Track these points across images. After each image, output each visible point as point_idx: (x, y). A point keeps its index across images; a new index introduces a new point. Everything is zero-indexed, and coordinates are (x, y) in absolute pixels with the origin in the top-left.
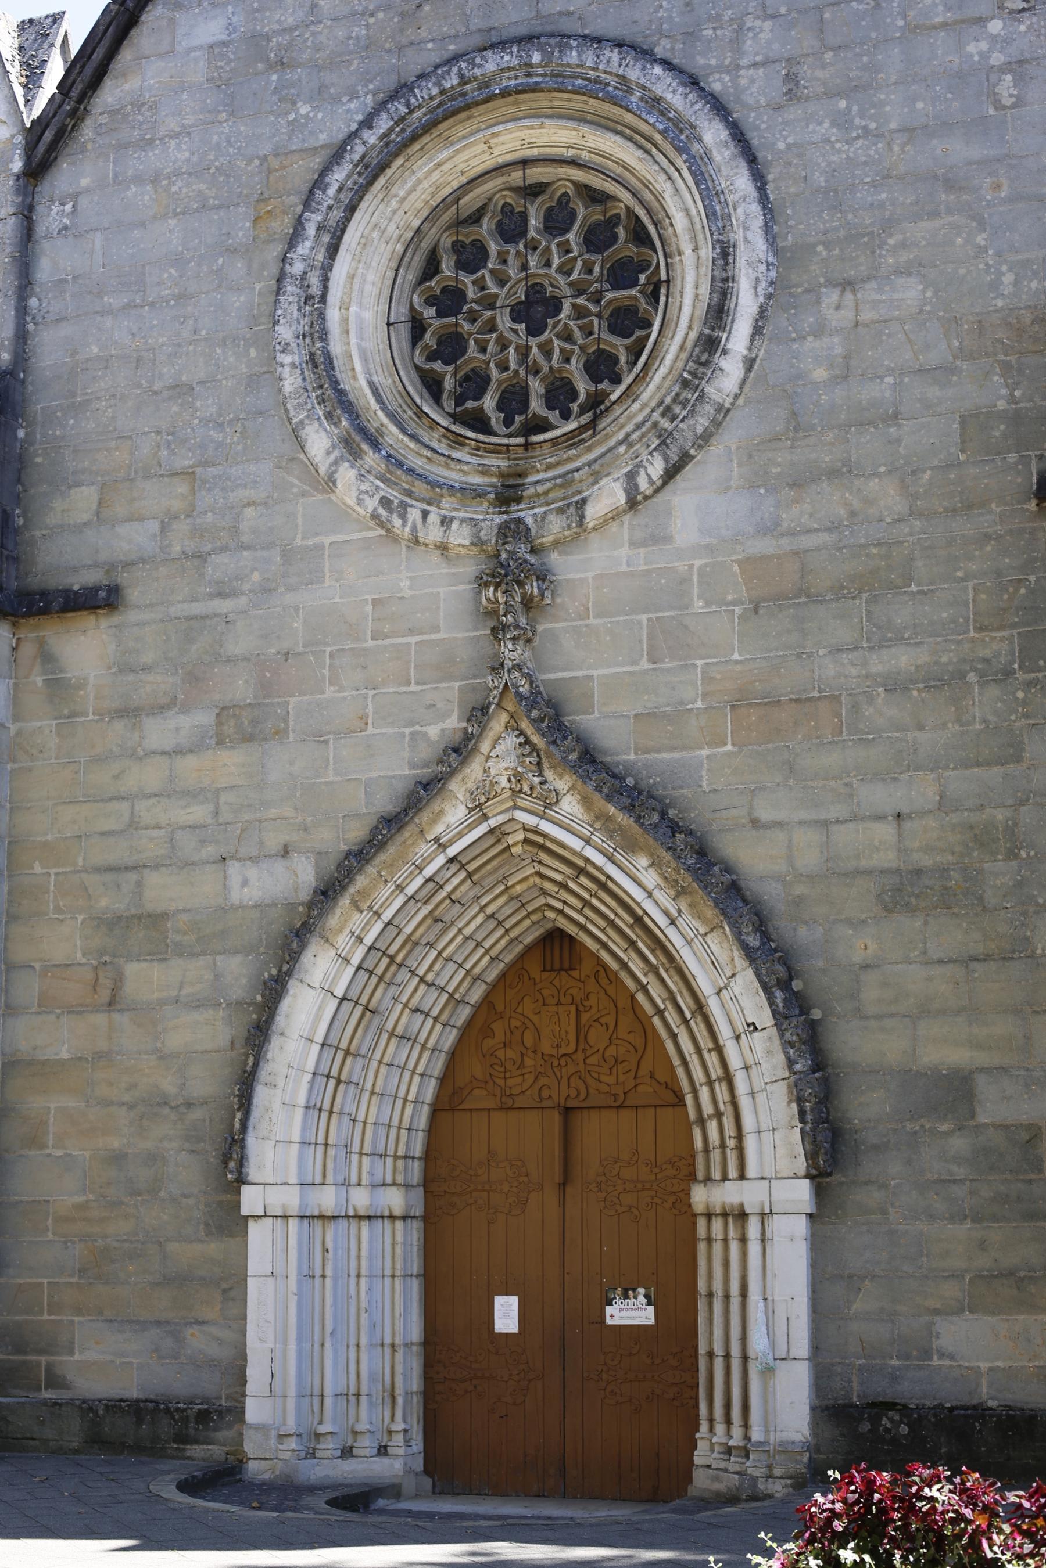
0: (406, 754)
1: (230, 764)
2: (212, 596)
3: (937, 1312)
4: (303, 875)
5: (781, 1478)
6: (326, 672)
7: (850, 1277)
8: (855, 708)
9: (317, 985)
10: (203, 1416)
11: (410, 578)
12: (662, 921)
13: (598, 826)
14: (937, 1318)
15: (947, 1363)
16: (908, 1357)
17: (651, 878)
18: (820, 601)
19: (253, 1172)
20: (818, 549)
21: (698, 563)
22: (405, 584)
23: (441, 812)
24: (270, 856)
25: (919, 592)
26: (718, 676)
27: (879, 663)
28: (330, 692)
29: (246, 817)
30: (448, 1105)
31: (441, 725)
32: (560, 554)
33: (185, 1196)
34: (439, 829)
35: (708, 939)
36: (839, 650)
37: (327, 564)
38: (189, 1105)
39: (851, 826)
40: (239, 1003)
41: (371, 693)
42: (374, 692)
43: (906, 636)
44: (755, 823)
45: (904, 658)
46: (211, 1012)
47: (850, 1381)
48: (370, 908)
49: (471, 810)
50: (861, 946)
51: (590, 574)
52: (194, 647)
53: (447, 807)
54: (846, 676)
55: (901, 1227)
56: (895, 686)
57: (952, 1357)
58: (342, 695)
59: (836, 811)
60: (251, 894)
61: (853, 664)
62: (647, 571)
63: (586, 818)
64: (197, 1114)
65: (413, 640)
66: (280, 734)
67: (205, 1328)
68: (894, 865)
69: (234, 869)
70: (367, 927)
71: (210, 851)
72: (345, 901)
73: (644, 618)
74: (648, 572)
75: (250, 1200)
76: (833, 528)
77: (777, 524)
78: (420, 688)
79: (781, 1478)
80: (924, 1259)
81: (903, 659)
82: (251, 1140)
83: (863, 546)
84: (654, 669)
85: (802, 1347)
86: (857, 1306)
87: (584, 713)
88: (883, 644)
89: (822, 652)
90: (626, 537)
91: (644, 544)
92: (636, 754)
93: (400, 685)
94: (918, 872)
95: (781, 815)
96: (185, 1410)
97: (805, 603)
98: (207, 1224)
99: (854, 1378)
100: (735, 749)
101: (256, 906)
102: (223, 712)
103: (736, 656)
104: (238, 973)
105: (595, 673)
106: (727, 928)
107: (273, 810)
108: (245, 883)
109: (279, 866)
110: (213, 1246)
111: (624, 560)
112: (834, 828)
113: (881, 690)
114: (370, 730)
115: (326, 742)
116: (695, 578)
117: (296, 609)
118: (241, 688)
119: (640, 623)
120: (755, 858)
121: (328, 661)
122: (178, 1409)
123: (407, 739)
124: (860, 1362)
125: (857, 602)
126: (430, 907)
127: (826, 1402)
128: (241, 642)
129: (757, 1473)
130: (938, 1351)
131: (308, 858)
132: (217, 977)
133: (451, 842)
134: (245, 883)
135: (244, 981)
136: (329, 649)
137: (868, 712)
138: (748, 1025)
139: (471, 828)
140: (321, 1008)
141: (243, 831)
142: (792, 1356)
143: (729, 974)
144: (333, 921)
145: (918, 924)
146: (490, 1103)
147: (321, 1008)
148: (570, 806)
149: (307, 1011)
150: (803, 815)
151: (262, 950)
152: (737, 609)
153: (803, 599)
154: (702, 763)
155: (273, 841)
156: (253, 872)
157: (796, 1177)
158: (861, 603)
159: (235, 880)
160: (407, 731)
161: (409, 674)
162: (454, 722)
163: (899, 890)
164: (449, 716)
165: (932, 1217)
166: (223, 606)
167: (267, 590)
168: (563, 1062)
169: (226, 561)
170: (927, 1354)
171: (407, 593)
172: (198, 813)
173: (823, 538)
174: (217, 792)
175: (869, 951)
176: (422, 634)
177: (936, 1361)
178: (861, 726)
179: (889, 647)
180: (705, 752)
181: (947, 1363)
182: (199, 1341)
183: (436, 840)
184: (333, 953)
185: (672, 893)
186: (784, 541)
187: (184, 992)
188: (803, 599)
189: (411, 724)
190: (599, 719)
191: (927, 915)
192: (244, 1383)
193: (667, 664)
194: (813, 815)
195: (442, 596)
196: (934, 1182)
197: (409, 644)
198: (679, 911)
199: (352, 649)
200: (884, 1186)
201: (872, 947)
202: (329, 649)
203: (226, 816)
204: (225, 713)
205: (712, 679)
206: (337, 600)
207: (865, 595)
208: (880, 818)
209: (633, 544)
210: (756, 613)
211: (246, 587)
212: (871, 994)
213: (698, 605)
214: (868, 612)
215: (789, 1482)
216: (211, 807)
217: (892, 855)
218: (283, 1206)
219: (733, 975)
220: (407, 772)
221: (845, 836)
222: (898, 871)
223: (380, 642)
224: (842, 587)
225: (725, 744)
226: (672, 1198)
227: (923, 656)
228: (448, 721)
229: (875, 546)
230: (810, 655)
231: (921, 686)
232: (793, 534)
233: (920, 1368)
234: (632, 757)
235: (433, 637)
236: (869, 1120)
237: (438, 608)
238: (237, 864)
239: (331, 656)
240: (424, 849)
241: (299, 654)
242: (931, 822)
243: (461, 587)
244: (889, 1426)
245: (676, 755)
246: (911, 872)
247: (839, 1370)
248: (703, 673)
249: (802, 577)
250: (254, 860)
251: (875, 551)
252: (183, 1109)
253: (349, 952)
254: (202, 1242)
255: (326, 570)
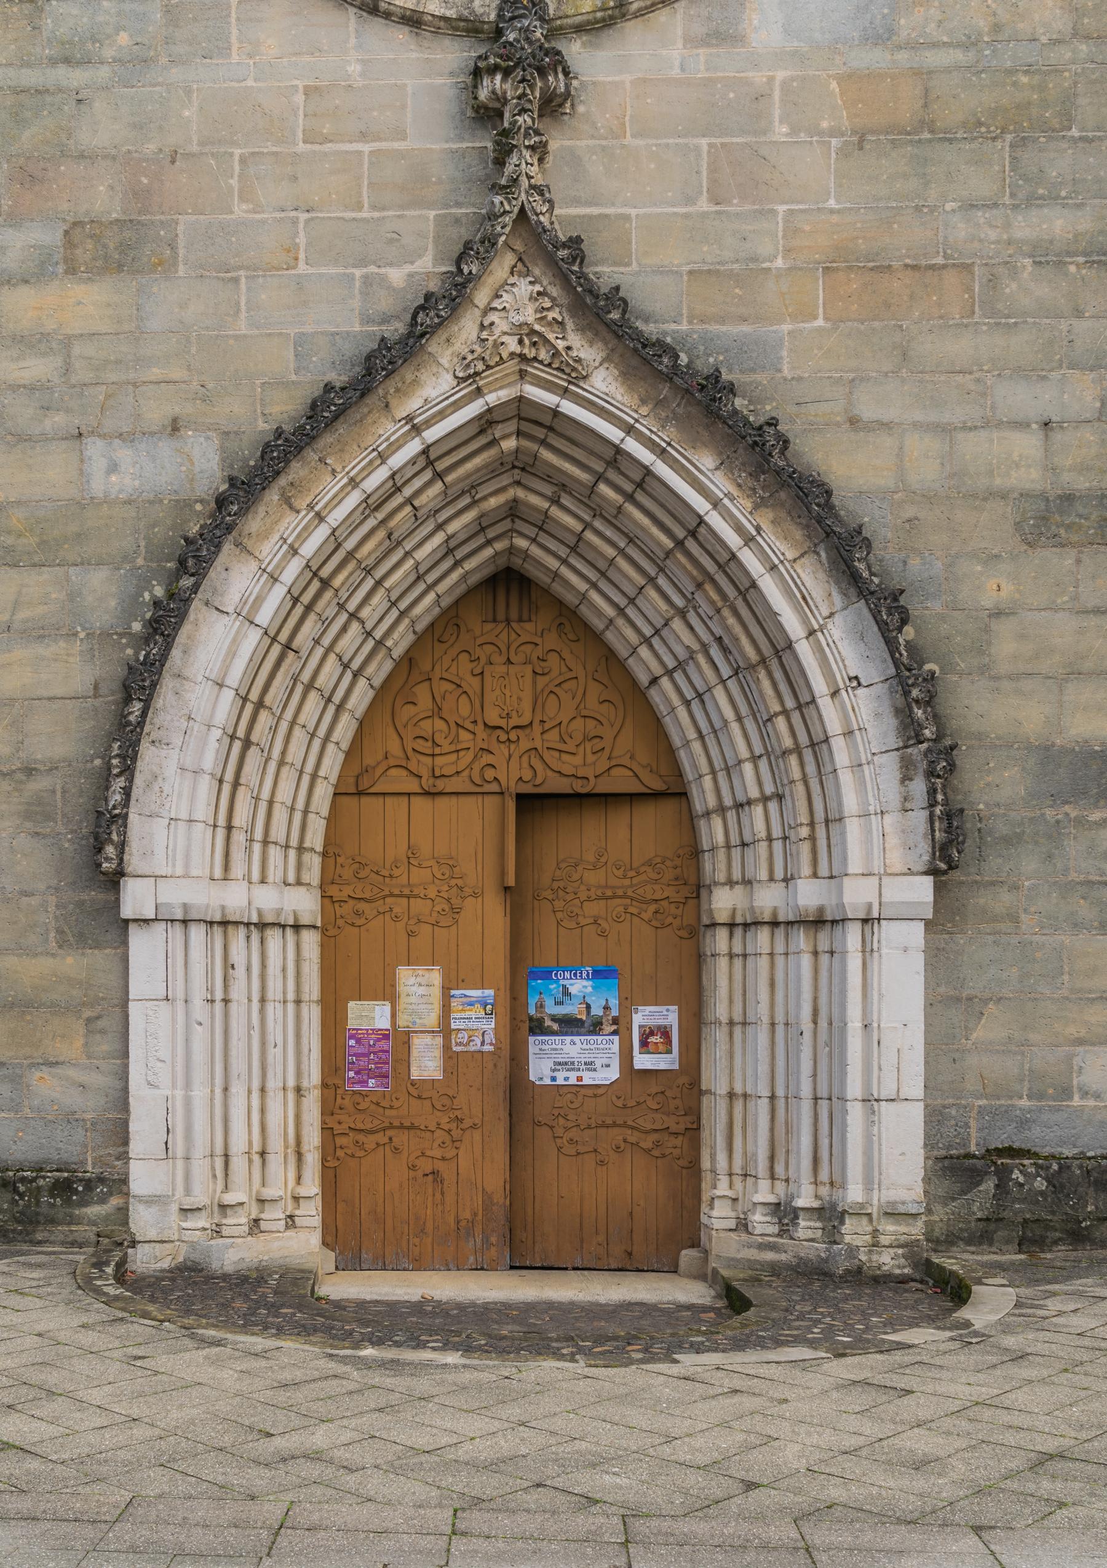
0: (356, 303)
1: (84, 305)
2: (53, 62)
3: (1080, 1042)
4: (201, 464)
5: (890, 1246)
6: (234, 182)
7: (970, 999)
8: (993, 281)
9: (230, 610)
10: (64, 1188)
11: (363, 62)
12: (733, 540)
13: (644, 410)
14: (1080, 1049)
15: (1091, 1103)
16: (1041, 1096)
17: (721, 484)
18: (950, 141)
19: (134, 861)
20: (948, 70)
21: (781, 75)
22: (354, 68)
23: (416, 382)
24: (152, 434)
25: (1081, 138)
26: (807, 228)
27: (1027, 226)
28: (240, 210)
29: (112, 377)
30: (354, 788)
31: (408, 268)
32: (584, 45)
33: (25, 893)
34: (413, 404)
35: (797, 566)
36: (972, 206)
37: (235, 32)
38: (29, 771)
39: (983, 434)
40: (105, 635)
41: (303, 217)
42: (307, 215)
43: (1063, 194)
44: (854, 422)
45: (1059, 223)
46: (62, 644)
47: (967, 1125)
48: (310, 507)
49: (461, 380)
50: (993, 587)
51: (627, 78)
52: (27, 134)
53: (424, 376)
54: (981, 241)
55: (1036, 938)
56: (1048, 257)
57: (1097, 1096)
58: (258, 216)
59: (955, 414)
60: (123, 483)
61: (991, 226)
62: (710, 79)
63: (626, 399)
64: (40, 784)
65: (366, 148)
66: (165, 266)
67: (58, 1070)
68: (1038, 487)
69: (95, 448)
70: (305, 534)
71: (58, 420)
72: (273, 496)
73: (704, 142)
74: (710, 82)
75: (136, 898)
76: (970, 43)
77: (891, 32)
78: (376, 214)
79: (890, 1246)
80: (1066, 977)
81: (1057, 224)
82: (133, 818)
83: (1010, 72)
84: (718, 213)
85: (915, 1087)
86: (979, 1034)
87: (615, 264)
88: (1032, 201)
89: (949, 206)
90: (679, 32)
91: (705, 41)
92: (690, 322)
93: (346, 208)
94: (1068, 498)
95: (890, 414)
96: (34, 1180)
97: (930, 141)
98: (60, 931)
99: (973, 1123)
100: (829, 325)
101: (128, 502)
102: (74, 231)
103: (832, 203)
104: (103, 595)
105: (633, 212)
106: (823, 554)
107: (155, 370)
108: (113, 468)
109: (165, 448)
110: (70, 960)
111: (677, 63)
112: (960, 436)
113: (1028, 261)
114: (302, 268)
115: (236, 280)
116: (777, 94)
117: (188, 92)
118: (103, 198)
119: (697, 149)
120: (853, 469)
121: (237, 168)
122: (23, 1180)
123: (357, 284)
124: (980, 1102)
125: (999, 144)
126: (380, 516)
127: (935, 1153)
128: (102, 128)
129: (858, 1241)
130: (1080, 1089)
131: (208, 438)
132: (72, 597)
133: (429, 423)
134: (113, 468)
135: (113, 603)
136: (237, 152)
137: (1011, 287)
138: (850, 679)
139: (457, 406)
140: (235, 643)
141: (108, 397)
142: (902, 1096)
143: (826, 613)
144: (253, 523)
145: (1069, 562)
146: (413, 786)
147: (235, 643)
148: (603, 382)
149: (217, 649)
150: (918, 416)
151: (140, 561)
152: (834, 141)
153: (927, 135)
154: (781, 339)
155: (156, 413)
156: (124, 454)
157: (910, 872)
158: (1004, 145)
159: (97, 464)
160: (358, 273)
161: (360, 194)
162: (427, 266)
163: (1044, 518)
164: (420, 256)
165: (1077, 926)
166: (75, 77)
167: (139, 61)
168: (513, 737)
169: (75, 12)
170: (1066, 1092)
171: (359, 83)
172: (37, 368)
173: (959, 56)
174: (67, 342)
175: (1002, 593)
176: (380, 139)
177: (1076, 1101)
178: (1000, 306)
179: (1040, 206)
180: (786, 327)
181: (1091, 1103)
182: (47, 1088)
183: (409, 419)
184: (253, 565)
185: (749, 505)
186: (902, 56)
187: (21, 615)
188: (927, 135)
189: (362, 262)
190: (637, 274)
191: (1080, 552)
192: (126, 1142)
193: (735, 207)
194: (933, 417)
195: (409, 89)
196: (1081, 883)
197: (360, 153)
198: (758, 529)
199: (276, 154)
200: (1015, 887)
201: (1008, 588)
202: (237, 152)
203: (82, 374)
204: (78, 230)
205: (796, 231)
206: (250, 83)
207: (1009, 137)
208: (1021, 425)
209: (690, 41)
210: (861, 148)
211: (108, 53)
212: (1005, 646)
213: (781, 131)
214: (1014, 159)
215: (900, 1251)
216: (59, 361)
217: (1035, 474)
218: (185, 906)
219: (832, 615)
220: (358, 329)
221: (976, 448)
222: (1043, 497)
223: (317, 147)
224: (980, 124)
225: (815, 318)
226: (653, 907)
227: (1085, 222)
228: (418, 263)
229: (1026, 72)
230: (933, 209)
231: (1081, 259)
232: (913, 46)
233: (1058, 1109)
234: (684, 327)
235: (396, 145)
236: (998, 805)
237: (404, 107)
238: (100, 443)
239: (243, 160)
240: (388, 429)
241: (193, 155)
242: (1089, 435)
243: (440, 81)
244: (1021, 1179)
245: (746, 328)
246: (1060, 497)
247: (954, 1112)
248: (786, 221)
249: (926, 105)
250: (127, 438)
251: (1025, 79)
252: (20, 776)
253: (277, 566)
254: (53, 955)
255: (234, 39)
